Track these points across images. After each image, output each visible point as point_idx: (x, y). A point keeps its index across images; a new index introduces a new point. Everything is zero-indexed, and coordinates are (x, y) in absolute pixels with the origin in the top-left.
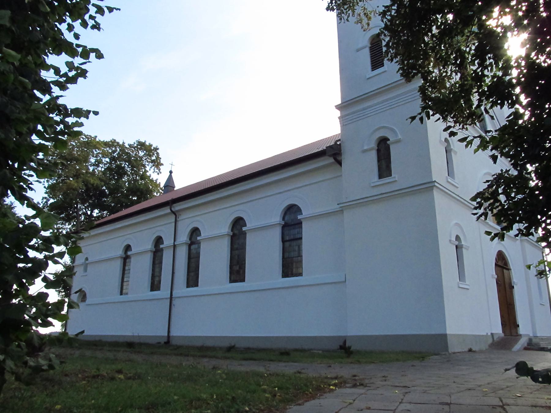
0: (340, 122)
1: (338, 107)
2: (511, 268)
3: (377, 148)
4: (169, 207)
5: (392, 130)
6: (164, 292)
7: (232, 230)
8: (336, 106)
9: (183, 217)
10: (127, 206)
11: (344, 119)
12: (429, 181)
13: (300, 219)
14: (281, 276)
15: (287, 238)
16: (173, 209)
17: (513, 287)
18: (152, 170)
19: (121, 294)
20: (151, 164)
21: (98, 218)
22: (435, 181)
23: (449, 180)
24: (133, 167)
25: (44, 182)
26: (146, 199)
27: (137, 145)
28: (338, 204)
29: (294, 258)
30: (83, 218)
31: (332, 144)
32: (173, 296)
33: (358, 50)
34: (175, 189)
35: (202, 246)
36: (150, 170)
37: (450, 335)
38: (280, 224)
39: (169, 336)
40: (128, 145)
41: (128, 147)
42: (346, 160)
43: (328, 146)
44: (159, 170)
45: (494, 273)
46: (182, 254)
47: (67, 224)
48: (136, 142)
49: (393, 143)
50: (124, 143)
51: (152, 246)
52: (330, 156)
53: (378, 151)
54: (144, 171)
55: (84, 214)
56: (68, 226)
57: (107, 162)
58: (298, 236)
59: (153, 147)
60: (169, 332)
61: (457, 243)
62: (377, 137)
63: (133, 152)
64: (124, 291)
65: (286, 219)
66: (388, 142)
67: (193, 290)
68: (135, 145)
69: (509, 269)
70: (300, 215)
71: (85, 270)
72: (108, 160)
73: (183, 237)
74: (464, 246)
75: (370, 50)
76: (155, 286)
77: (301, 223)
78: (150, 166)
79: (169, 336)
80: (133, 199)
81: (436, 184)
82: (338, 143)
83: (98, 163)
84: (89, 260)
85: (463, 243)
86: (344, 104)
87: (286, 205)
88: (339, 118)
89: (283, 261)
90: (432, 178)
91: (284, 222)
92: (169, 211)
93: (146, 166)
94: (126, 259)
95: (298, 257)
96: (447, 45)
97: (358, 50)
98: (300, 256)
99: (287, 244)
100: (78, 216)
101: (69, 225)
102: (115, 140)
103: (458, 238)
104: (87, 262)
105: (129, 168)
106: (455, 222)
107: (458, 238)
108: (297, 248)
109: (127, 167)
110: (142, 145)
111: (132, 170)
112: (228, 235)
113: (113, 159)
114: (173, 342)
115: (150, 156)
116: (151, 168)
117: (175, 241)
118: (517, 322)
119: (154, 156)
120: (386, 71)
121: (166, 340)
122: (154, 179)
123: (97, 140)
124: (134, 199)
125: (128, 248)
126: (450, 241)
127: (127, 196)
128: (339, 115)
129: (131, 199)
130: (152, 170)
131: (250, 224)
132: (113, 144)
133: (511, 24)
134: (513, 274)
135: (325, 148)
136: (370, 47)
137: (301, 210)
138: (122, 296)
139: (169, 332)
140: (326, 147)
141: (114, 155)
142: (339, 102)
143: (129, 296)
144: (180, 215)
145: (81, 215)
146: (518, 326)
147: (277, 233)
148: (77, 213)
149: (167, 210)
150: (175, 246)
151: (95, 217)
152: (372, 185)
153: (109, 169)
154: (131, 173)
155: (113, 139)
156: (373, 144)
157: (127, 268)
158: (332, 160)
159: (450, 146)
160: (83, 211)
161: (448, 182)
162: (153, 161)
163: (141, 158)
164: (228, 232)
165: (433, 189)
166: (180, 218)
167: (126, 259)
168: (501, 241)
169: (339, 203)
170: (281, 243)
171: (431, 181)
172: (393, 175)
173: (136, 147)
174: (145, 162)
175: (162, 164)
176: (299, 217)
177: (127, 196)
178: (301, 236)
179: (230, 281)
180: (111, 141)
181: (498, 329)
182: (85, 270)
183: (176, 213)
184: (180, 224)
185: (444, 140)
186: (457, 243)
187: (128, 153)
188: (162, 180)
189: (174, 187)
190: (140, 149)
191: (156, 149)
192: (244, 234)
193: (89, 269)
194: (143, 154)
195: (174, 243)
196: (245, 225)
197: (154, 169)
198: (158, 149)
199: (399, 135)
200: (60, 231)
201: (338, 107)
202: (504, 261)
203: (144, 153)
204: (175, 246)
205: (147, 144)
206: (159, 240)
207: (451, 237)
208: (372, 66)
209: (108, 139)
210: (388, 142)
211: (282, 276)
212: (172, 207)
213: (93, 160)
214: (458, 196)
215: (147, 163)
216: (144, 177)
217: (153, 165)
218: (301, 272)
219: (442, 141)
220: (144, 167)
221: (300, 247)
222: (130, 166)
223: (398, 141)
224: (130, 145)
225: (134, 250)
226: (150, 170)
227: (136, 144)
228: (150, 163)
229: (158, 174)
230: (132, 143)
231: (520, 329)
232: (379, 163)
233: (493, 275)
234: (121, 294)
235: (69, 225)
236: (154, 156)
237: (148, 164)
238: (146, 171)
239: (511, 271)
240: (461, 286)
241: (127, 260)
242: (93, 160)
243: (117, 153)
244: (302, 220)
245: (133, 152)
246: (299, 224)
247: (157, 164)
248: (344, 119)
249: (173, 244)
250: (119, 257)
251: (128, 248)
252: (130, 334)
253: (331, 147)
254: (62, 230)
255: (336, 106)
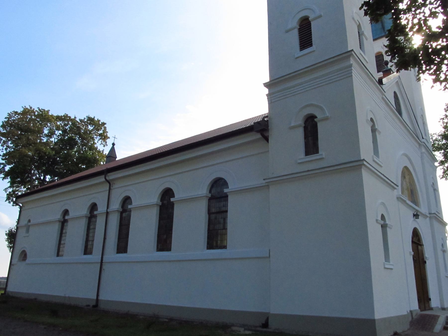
0: (268, 99)
1: (266, 85)
2: (424, 244)
3: (303, 125)
4: (103, 176)
5: (321, 108)
6: (95, 257)
7: (162, 200)
8: (264, 84)
9: (116, 185)
10: (73, 173)
11: (272, 96)
12: (357, 159)
13: (226, 193)
14: (206, 248)
15: (213, 210)
16: (107, 178)
17: (425, 262)
18: (100, 142)
19: (58, 255)
20: (99, 137)
21: (50, 182)
22: (364, 160)
23: (375, 159)
24: (83, 139)
25: (3, 149)
26: (92, 167)
27: (87, 120)
28: (264, 180)
29: (219, 231)
30: (37, 182)
31: (259, 120)
32: (103, 261)
33: (287, 31)
34: (117, 159)
35: (133, 214)
36: (98, 142)
37: (379, 320)
38: (207, 196)
39: (97, 300)
40: (79, 119)
41: (79, 121)
42: (273, 134)
43: (256, 121)
44: (106, 142)
45: (411, 251)
46: (114, 221)
47: (22, 187)
48: (86, 118)
49: (320, 121)
50: (75, 118)
51: (87, 212)
52: (258, 132)
53: (305, 128)
54: (92, 143)
55: (37, 178)
56: (23, 189)
57: (60, 134)
58: (224, 209)
59: (101, 122)
60: (98, 295)
61: (382, 222)
62: (305, 114)
63: (83, 126)
64: (60, 253)
65: (213, 192)
66: (316, 120)
67: (122, 256)
68: (86, 120)
69: (422, 245)
70: (226, 188)
71: (28, 231)
72: (60, 132)
73: (116, 205)
74: (388, 225)
75: (299, 31)
76: (87, 251)
77: (227, 196)
78: (98, 139)
79: (97, 300)
80: (82, 167)
81: (365, 163)
82: (266, 119)
83: (51, 134)
84: (31, 222)
85: (387, 222)
86: (272, 82)
87: (214, 178)
88: (267, 95)
89: (208, 233)
90: (360, 157)
91: (210, 194)
92: (104, 180)
93: (95, 139)
94: (64, 223)
95: (223, 229)
96: (61, 329)
97: (287, 31)
98: (225, 228)
99: (213, 216)
100: (32, 181)
101: (24, 188)
102: (67, 115)
103: (383, 217)
104: (29, 224)
105: (80, 140)
106: (380, 201)
107: (383, 217)
108: (222, 221)
109: (78, 138)
110: (91, 120)
111: (82, 142)
112: (157, 205)
113: (65, 131)
114: (102, 306)
115: (98, 130)
116: (99, 140)
117: (108, 208)
118: (429, 296)
119: (102, 130)
120: (314, 51)
121: (94, 303)
122: (101, 150)
123: (50, 114)
124: (83, 167)
125: (66, 212)
126: (377, 220)
127: (77, 164)
128: (267, 92)
129: (80, 167)
130: (100, 142)
131: (178, 195)
132: (65, 118)
133: (409, 32)
134: (425, 248)
135: (252, 124)
136: (299, 29)
137: (227, 184)
138: (58, 258)
139: (98, 295)
140: (254, 123)
141: (67, 128)
142: (267, 80)
143: (64, 258)
144: (114, 184)
145: (35, 180)
146: (430, 299)
147: (203, 206)
148: (31, 178)
149: (101, 179)
150: (107, 213)
151: (48, 182)
152: (300, 161)
153: (61, 141)
154: (81, 144)
155: (65, 114)
156: (300, 121)
157: (64, 231)
158: (259, 136)
159: (375, 126)
160: (36, 176)
161: (374, 161)
162: (100, 135)
163: (90, 132)
164: (157, 202)
165: (361, 168)
166: (115, 186)
167: (64, 223)
168: (416, 218)
169: (265, 178)
170: (207, 215)
171: (360, 159)
172: (320, 152)
173: (86, 122)
174: (94, 135)
175: (109, 138)
176: (226, 191)
177: (77, 164)
178: (226, 209)
179: (157, 249)
180: (64, 116)
181: (415, 306)
182: (28, 231)
183: (110, 182)
184: (113, 192)
185: (370, 120)
186: (382, 222)
187: (79, 127)
188: (106, 151)
189: (116, 158)
190: (90, 124)
191: (104, 124)
192: (172, 204)
193: (31, 228)
194: (92, 128)
195: (107, 210)
196: (228, 187)
197: (102, 141)
198: (105, 124)
199: (327, 112)
200: (16, 193)
201: (266, 85)
202: (417, 238)
203: (93, 128)
204: (107, 213)
205: (96, 119)
206: (94, 207)
207: (377, 217)
208: (300, 47)
209: (61, 114)
210: (316, 120)
211: (207, 247)
212: (107, 176)
213: (46, 131)
214: (383, 175)
215: (95, 136)
216: (92, 148)
217: (101, 139)
218: (225, 245)
219: (368, 120)
220: (94, 140)
221: (225, 219)
222: (80, 139)
223: (326, 119)
224: (81, 120)
225: (72, 214)
226: (98, 142)
227: (86, 119)
228: (98, 136)
229: (104, 146)
230: (83, 119)
231: (432, 303)
232: (306, 140)
233: (410, 252)
234: (58, 255)
235: (24, 188)
236: (102, 130)
237: (96, 137)
238: (94, 143)
239: (423, 246)
240: (387, 266)
241: (65, 224)
242: (46, 131)
243: (69, 126)
244: (228, 194)
245: (83, 126)
246: (225, 197)
247: (104, 137)
248: (272, 96)
249: (106, 211)
250: (57, 221)
251: (66, 212)
252: (62, 295)
253: (258, 123)
254: (17, 192)
255: (264, 84)
